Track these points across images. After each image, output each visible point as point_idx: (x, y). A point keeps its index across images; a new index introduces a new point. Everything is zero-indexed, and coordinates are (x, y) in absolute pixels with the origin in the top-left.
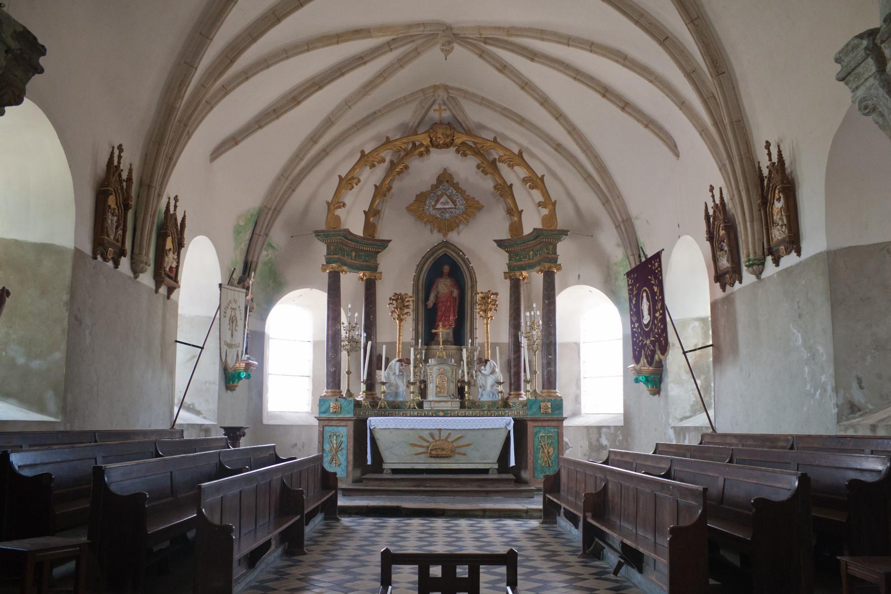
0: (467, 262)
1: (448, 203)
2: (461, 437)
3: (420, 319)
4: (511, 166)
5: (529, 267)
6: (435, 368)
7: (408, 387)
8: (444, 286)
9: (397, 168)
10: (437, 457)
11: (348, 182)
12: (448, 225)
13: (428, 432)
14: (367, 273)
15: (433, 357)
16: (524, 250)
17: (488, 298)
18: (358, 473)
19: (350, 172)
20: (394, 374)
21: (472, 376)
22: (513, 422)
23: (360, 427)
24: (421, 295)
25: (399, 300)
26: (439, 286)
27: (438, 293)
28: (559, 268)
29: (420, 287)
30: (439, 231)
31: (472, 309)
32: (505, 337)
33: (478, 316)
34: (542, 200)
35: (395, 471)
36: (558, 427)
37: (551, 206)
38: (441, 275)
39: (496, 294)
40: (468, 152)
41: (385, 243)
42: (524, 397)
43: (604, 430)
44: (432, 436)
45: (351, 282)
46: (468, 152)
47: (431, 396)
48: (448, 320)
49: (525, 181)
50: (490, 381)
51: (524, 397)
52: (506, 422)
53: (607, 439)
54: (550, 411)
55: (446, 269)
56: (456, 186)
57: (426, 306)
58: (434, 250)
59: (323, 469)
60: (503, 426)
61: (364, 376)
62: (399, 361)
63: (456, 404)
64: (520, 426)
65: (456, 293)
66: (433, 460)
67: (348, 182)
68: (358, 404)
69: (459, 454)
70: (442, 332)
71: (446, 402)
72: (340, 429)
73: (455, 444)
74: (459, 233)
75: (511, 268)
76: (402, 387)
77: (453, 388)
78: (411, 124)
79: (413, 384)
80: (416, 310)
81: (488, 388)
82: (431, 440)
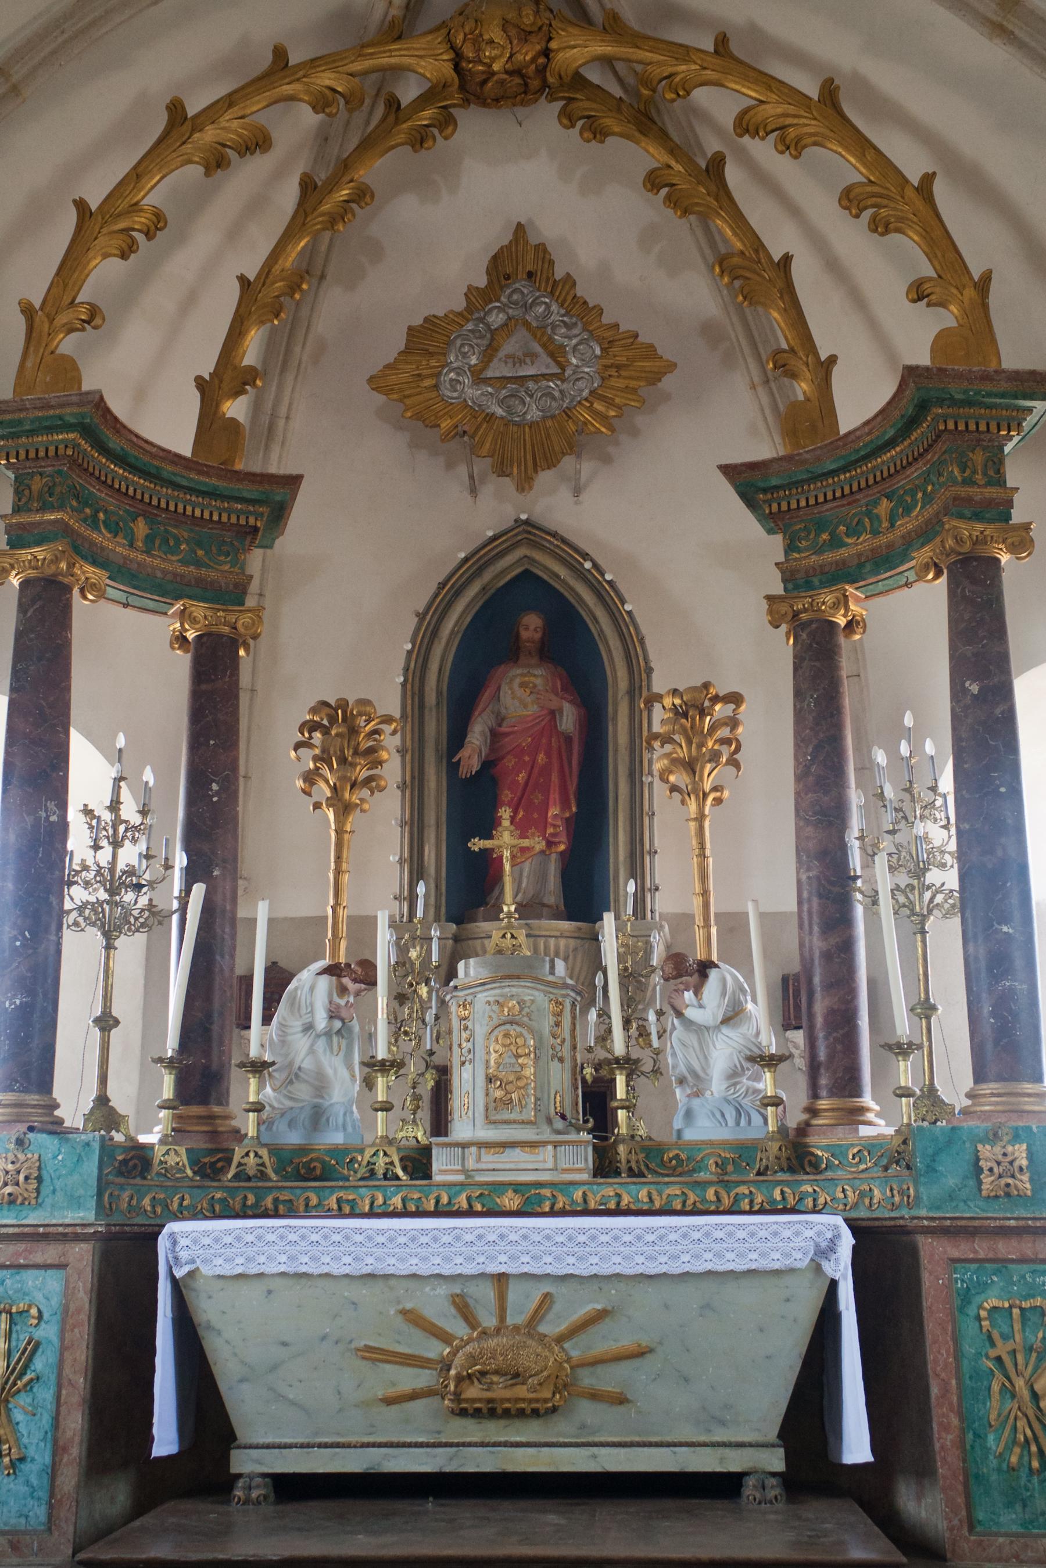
0: (608, 596)
1: (533, 356)
2: (600, 1316)
3: (430, 818)
4: (792, 146)
5: (881, 564)
7: (369, 1084)
8: (523, 695)
9: (329, 204)
10: (491, 1411)
11: (113, 225)
12: (527, 450)
13: (443, 1290)
14: (199, 610)
16: (848, 497)
17: (703, 713)
18: (117, 1495)
20: (309, 1027)
21: (644, 1033)
22: (847, 1241)
23: (126, 1269)
24: (435, 727)
25: (339, 731)
27: (500, 720)
28: (1021, 541)
29: (431, 698)
30: (502, 471)
33: (660, 789)
35: (291, 1488)
37: (970, 293)
38: (511, 652)
39: (735, 699)
42: (878, 1126)
44: (463, 1308)
46: (609, 122)
47: (461, 1129)
48: (542, 825)
49: (851, 200)
50: (718, 1062)
52: (809, 1243)
54: (1024, 1182)
55: (531, 626)
56: (563, 290)
57: (453, 768)
58: (478, 561)
60: (801, 1261)
62: (332, 970)
63: (575, 1159)
64: (884, 1257)
65: (569, 719)
66: (472, 1430)
68: (136, 1161)
69: (595, 1396)
71: (533, 1145)
72: (31, 1279)
73: (575, 1350)
74: (577, 492)
75: (796, 580)
76: (343, 1085)
80: (414, 786)
81: (717, 1086)
82: (459, 1329)
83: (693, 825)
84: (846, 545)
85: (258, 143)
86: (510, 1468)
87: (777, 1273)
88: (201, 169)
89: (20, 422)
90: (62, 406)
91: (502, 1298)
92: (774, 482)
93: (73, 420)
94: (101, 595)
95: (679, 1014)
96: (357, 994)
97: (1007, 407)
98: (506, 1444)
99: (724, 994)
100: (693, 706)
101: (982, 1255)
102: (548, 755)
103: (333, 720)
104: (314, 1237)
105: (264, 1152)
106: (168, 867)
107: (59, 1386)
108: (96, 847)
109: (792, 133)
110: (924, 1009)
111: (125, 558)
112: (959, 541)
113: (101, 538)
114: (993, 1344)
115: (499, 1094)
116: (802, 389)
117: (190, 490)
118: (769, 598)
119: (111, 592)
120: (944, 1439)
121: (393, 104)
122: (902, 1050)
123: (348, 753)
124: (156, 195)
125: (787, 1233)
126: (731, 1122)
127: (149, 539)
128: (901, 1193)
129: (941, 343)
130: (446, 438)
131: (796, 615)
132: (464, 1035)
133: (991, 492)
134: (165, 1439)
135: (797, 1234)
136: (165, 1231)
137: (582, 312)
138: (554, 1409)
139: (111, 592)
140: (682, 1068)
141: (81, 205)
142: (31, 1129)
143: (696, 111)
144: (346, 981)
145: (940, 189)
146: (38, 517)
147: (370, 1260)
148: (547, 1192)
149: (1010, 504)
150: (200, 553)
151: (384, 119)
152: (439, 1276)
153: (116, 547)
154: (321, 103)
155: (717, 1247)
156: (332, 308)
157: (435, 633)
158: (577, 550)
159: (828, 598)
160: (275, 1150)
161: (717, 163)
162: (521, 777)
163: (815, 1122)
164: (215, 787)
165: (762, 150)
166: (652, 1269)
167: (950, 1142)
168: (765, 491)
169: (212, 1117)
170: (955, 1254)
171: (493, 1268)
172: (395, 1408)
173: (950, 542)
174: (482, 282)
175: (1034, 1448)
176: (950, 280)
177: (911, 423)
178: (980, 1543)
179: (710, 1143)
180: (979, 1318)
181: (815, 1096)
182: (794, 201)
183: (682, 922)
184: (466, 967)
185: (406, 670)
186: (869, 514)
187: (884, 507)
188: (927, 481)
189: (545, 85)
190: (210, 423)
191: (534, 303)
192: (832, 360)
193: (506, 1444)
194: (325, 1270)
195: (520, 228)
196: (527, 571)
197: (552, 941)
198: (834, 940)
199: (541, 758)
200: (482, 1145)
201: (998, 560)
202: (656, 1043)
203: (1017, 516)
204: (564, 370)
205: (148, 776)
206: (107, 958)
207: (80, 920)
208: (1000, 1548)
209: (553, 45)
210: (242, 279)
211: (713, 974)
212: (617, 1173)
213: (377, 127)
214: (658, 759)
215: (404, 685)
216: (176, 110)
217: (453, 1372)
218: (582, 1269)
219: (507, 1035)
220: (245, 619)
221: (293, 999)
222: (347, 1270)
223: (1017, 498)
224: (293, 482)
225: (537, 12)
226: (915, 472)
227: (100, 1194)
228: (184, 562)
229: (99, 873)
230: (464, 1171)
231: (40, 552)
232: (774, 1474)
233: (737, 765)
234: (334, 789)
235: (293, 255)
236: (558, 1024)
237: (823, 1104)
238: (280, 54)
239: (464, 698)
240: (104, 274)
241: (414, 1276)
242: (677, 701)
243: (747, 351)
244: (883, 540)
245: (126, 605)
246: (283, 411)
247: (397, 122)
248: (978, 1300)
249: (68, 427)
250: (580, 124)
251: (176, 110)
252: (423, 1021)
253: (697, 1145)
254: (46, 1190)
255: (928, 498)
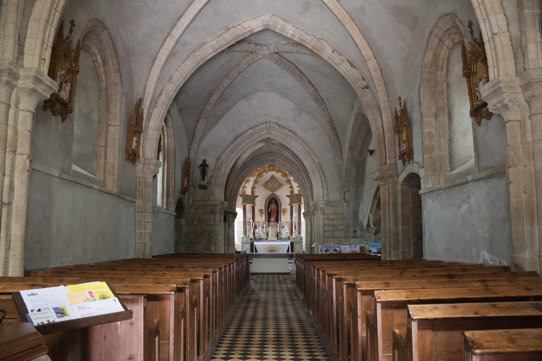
0: (279, 199)
8: (273, 206)
23: (252, 245)
25: (261, 211)
32: (289, 220)
38: (272, 203)
41: (257, 196)
45: (249, 207)
47: (270, 236)
50: (285, 232)
51: (294, 236)
52: (288, 243)
55: (273, 201)
56: (276, 180)
58: (270, 196)
61: (252, 231)
63: (276, 239)
64: (292, 244)
65: (276, 208)
68: (251, 239)
70: (272, 219)
76: (262, 234)
77: (275, 234)
239: (269, 206)
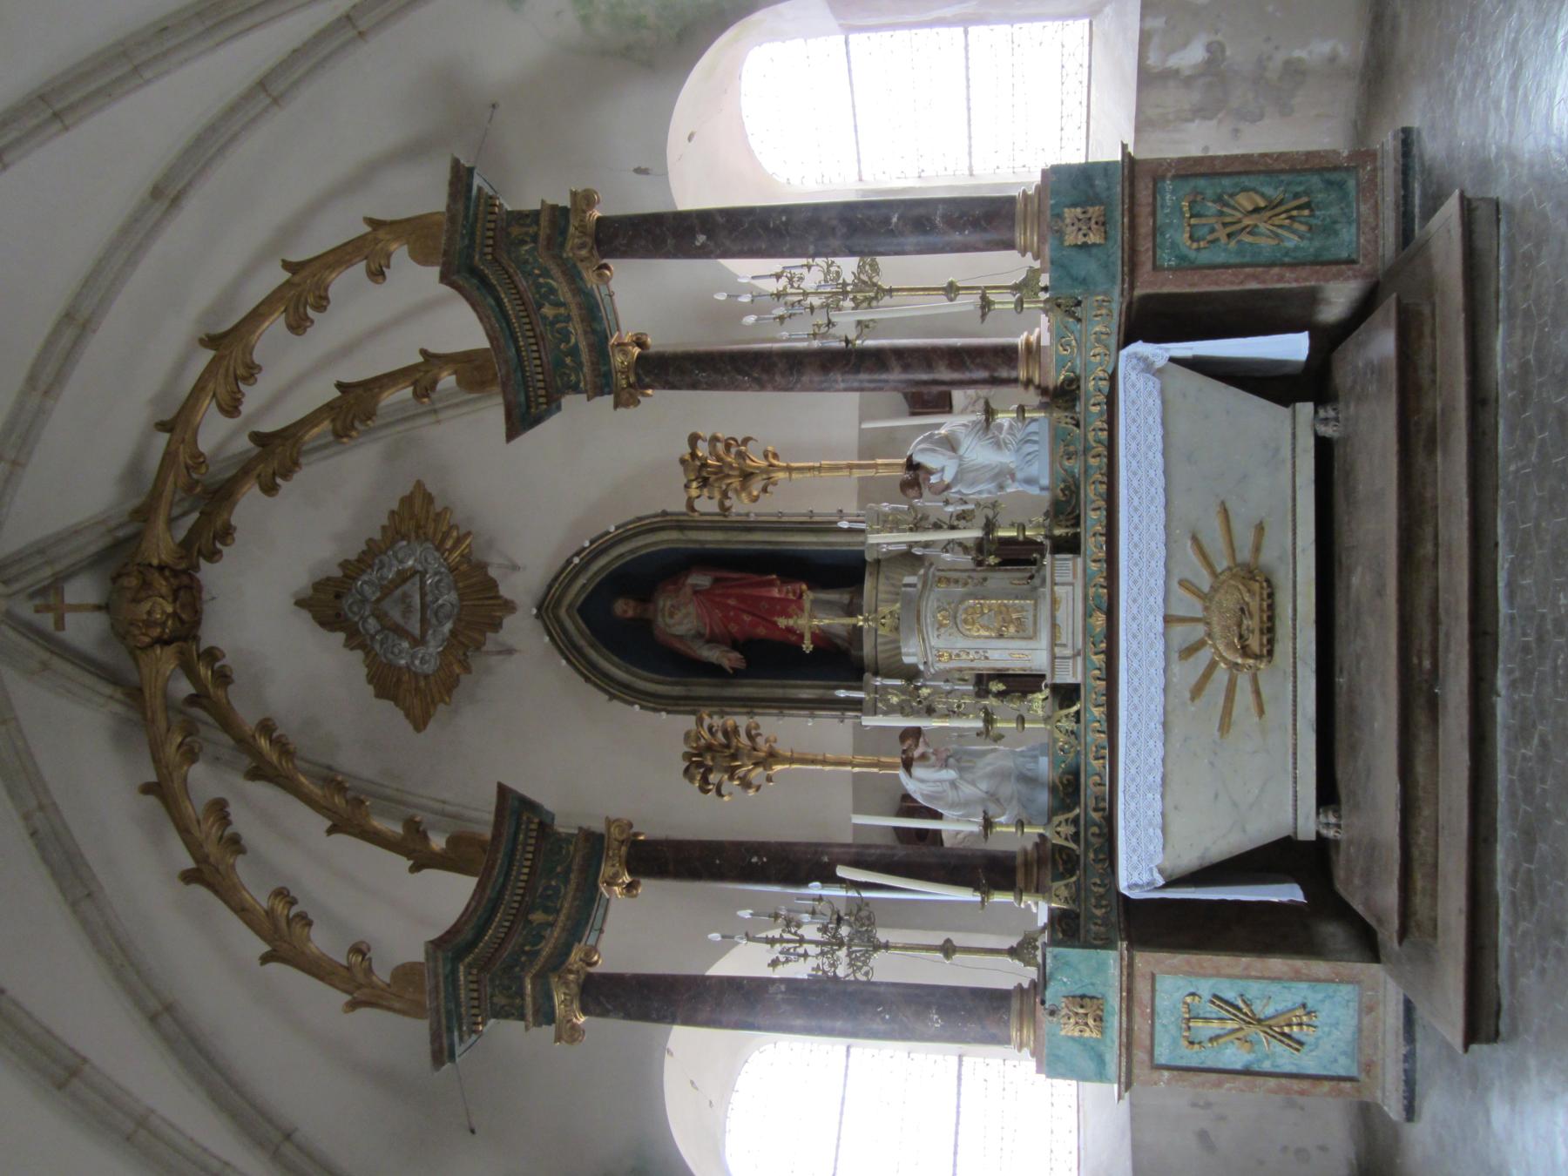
1: (405, 596)
2: (1195, 539)
3: (779, 693)
4: (251, 372)
5: (593, 313)
6: (934, 642)
7: (999, 738)
8: (680, 618)
9: (271, 759)
10: (1269, 630)
11: (283, 935)
12: (481, 604)
13: (1176, 668)
14: (606, 870)
15: (897, 652)
17: (705, 465)
19: (250, 924)
20: (953, 784)
21: (962, 516)
22: (1139, 347)
25: (709, 761)
26: (680, 630)
28: (586, 199)
29: (677, 690)
30: (496, 626)
31: (748, 527)
34: (360, 268)
35: (1328, 795)
36: (1157, 179)
37: (381, 234)
39: (694, 439)
40: (219, 523)
42: (1040, 330)
43: (1153, 59)
44: (1190, 651)
45: (638, 928)
46: (219, 523)
47: (1030, 655)
49: (298, 325)
50: (991, 456)
51: (1040, 330)
52: (1143, 373)
53: (1184, 45)
54: (1094, 211)
55: (624, 608)
56: (353, 569)
57: (737, 674)
59: (1119, 894)
62: (908, 765)
63: (1067, 579)
64: (1151, 320)
65: (701, 580)
66: (1283, 647)
67: (283, 935)
68: (1066, 928)
69: (1257, 549)
70: (813, 618)
71: (1054, 602)
72: (1163, 1002)
75: (603, 384)
78: (119, 708)
79: (989, 719)
80: (751, 705)
82: (1205, 655)
83: (795, 475)
84: (576, 345)
85: (219, 809)
86: (1313, 616)
87: (1164, 402)
88: (240, 858)
89: (448, 1012)
90: (436, 976)
91: (1182, 620)
92: (522, 398)
93: (449, 967)
94: (594, 949)
95: (948, 487)
96: (927, 744)
97: (477, 206)
98: (1294, 620)
99: (933, 451)
100: (701, 473)
101: (1150, 245)
102: (729, 596)
103: (699, 765)
104: (1133, 771)
105: (1056, 820)
106: (820, 898)
107: (1248, 977)
108: (805, 955)
109: (241, 371)
110: (951, 290)
111: (563, 930)
112: (583, 246)
113: (546, 949)
114: (1216, 240)
115: (1012, 629)
116: (448, 381)
117: (507, 875)
118: (616, 406)
119: (591, 941)
120: (1290, 281)
121: (192, 700)
122: (986, 304)
123: (727, 752)
124: (260, 898)
125: (1133, 393)
126: (1036, 447)
127: (546, 910)
128: (1100, 307)
129: (421, 257)
130: (468, 670)
131: (630, 385)
132: (964, 656)
133: (544, 221)
134: (1289, 893)
135: (1133, 386)
136: (1126, 892)
137: (370, 556)
138: (1268, 581)
139: (591, 941)
140: (991, 486)
141: (265, 959)
142: (1043, 1002)
143: (221, 447)
144: (916, 754)
145: (296, 257)
146: (529, 1000)
147: (1152, 725)
148: (1091, 591)
149: (554, 208)
150: (559, 869)
151: (204, 708)
152: (1165, 670)
153: (555, 935)
154: (191, 756)
155: (1143, 448)
156: (354, 762)
157: (626, 687)
158: (564, 569)
159: (618, 360)
160: (1053, 812)
161: (257, 438)
162: (747, 618)
163: (1037, 381)
164: (755, 860)
165: (253, 397)
166: (1161, 499)
167: (1062, 266)
168: (529, 407)
169: (1027, 864)
170: (1149, 266)
171: (1159, 625)
172: (1266, 708)
173: (584, 253)
174: (340, 636)
175: (1295, 213)
176: (369, 250)
177: (484, 281)
178: (1365, 256)
179: (1052, 463)
180: (1198, 249)
181: (1016, 381)
182: (294, 376)
183: (866, 491)
184: (908, 655)
185: (655, 710)
186: (553, 324)
187: (548, 311)
188: (530, 274)
189: (185, 572)
190: (449, 861)
191: (361, 593)
192: (424, 352)
193: (1294, 620)
194: (1159, 762)
195: (301, 603)
196: (580, 611)
197: (881, 596)
198: (893, 362)
199: (732, 602)
200: (1053, 643)
201: (599, 219)
202: (970, 507)
203: (565, 201)
204: (416, 572)
205: (746, 914)
206: (896, 948)
207: (865, 969)
208: (1368, 241)
209: (155, 562)
210: (330, 831)
211: (917, 458)
212: (1077, 536)
213: (210, 714)
214: (740, 506)
215: (669, 712)
216: (188, 877)
217: (1240, 661)
218: (1161, 553)
219: (965, 621)
220: (615, 832)
221: (927, 797)
222: (1160, 744)
223: (550, 201)
224: (503, 791)
225: (128, 575)
226: (523, 284)
227: (1096, 947)
228: (567, 881)
229: (823, 953)
230: (1074, 656)
231: (558, 998)
232: (1316, 412)
233: (746, 441)
234: (756, 764)
235: (312, 787)
236: (957, 581)
237: (1022, 374)
238: (147, 789)
240: (322, 941)
241: (1165, 690)
242: (694, 485)
243: (407, 425)
244: (575, 312)
245: (601, 931)
246: (437, 806)
247: (208, 696)
248: (1185, 250)
249: (454, 971)
250: (219, 546)
251: (188, 877)
252: (949, 693)
253: (1053, 472)
254: (1091, 991)
255: (546, 273)
